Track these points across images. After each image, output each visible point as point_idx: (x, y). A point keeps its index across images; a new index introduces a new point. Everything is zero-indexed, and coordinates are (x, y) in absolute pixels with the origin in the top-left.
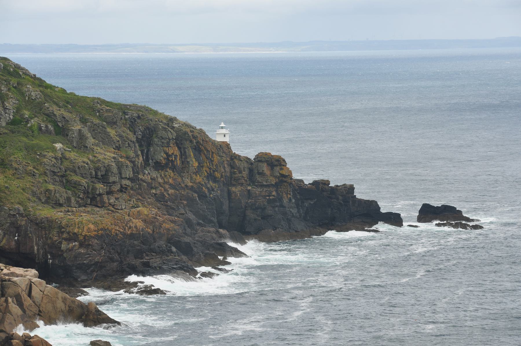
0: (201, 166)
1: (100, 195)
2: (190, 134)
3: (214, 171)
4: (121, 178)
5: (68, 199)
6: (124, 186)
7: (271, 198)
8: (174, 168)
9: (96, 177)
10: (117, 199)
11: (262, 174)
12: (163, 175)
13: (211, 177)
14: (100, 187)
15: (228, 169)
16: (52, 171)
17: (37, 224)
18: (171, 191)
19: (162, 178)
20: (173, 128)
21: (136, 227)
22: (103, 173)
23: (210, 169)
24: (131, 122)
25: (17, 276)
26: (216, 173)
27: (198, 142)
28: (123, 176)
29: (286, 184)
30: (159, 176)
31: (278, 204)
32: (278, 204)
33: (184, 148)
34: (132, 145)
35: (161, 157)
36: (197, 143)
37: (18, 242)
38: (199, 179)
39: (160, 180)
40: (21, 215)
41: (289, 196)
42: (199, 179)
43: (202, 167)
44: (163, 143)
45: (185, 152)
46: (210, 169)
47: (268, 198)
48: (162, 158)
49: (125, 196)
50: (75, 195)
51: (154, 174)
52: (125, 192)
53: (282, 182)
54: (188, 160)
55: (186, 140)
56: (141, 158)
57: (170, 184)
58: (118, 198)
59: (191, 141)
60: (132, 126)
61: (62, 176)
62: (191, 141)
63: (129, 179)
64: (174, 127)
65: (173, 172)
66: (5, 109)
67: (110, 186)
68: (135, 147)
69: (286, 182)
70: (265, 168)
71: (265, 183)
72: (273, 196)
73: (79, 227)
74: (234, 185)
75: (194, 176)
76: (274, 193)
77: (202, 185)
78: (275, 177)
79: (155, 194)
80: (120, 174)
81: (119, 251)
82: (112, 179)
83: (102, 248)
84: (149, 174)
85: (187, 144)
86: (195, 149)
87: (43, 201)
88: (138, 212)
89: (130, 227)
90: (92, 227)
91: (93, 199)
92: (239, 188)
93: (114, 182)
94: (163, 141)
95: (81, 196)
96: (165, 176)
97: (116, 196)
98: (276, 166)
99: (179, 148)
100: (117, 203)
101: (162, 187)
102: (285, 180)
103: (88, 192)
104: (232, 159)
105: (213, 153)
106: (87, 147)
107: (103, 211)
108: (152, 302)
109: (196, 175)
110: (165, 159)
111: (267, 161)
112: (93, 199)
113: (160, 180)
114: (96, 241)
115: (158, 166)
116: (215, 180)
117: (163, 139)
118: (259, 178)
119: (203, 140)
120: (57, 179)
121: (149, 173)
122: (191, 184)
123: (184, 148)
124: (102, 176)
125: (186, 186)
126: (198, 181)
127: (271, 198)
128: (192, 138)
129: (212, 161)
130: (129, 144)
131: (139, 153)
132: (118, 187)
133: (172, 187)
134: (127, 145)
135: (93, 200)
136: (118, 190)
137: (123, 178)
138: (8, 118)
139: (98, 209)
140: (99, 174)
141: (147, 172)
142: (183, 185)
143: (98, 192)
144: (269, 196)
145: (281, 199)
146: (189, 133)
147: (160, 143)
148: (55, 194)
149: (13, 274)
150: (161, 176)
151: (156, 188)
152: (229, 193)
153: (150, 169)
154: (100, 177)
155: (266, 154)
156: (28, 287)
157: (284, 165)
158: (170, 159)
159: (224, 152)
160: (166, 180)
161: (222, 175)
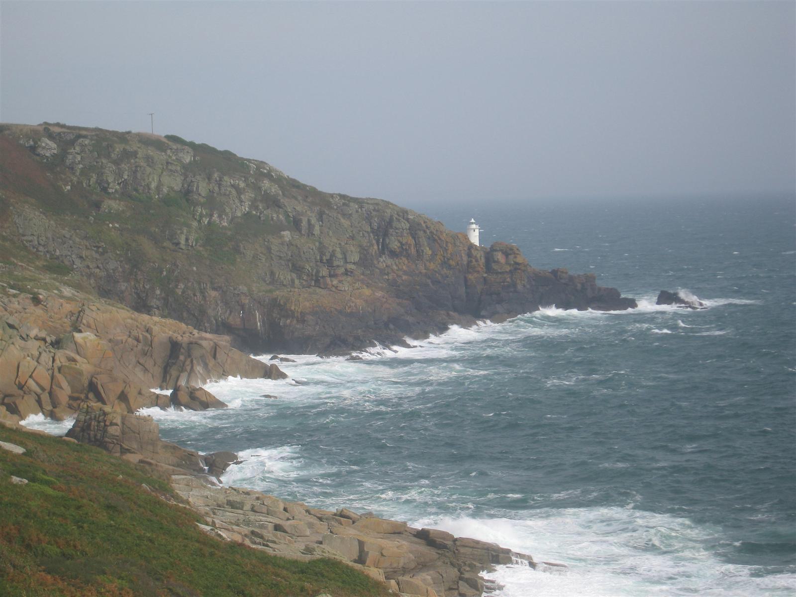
0: (434, 254)
1: (323, 277)
2: (424, 225)
3: (448, 259)
4: (346, 262)
5: (293, 281)
6: (349, 270)
7: (505, 284)
8: (408, 256)
9: (321, 261)
10: (340, 282)
11: (497, 262)
12: (397, 263)
13: (445, 263)
14: (324, 271)
15: (465, 258)
16: (278, 256)
17: (259, 302)
18: (404, 277)
19: (397, 265)
20: (408, 220)
21: (356, 306)
22: (328, 257)
23: (444, 257)
24: (368, 214)
25: (206, 339)
26: (451, 261)
27: (431, 232)
28: (348, 261)
29: (519, 271)
30: (393, 263)
31: (512, 290)
32: (512, 290)
33: (419, 238)
34: (366, 234)
35: (395, 245)
36: (431, 232)
37: (243, 319)
38: (432, 266)
39: (395, 267)
40: (245, 294)
41: (523, 282)
42: (432, 266)
43: (436, 255)
44: (397, 233)
45: (419, 242)
46: (444, 257)
47: (502, 284)
48: (396, 247)
49: (349, 279)
50: (300, 278)
51: (389, 261)
52: (350, 276)
53: (516, 269)
54: (422, 248)
55: (420, 230)
56: (376, 247)
57: (404, 271)
58: (342, 281)
59: (425, 232)
60: (368, 218)
61: (289, 260)
62: (425, 232)
63: (354, 263)
64: (409, 219)
65: (408, 259)
66: (241, 201)
67: (334, 270)
68: (369, 236)
69: (520, 269)
70: (500, 256)
71: (499, 271)
72: (508, 282)
73: (295, 305)
74: (470, 273)
75: (428, 264)
76: (508, 280)
77: (435, 271)
78: (510, 265)
79: (388, 280)
80: (346, 259)
81: (333, 327)
82: (336, 263)
83: (317, 324)
84: (385, 261)
85: (421, 233)
86: (429, 238)
87: (268, 282)
88: (360, 293)
89: (350, 307)
90: (307, 304)
91: (317, 281)
92: (476, 275)
93: (338, 266)
94: (397, 231)
95: (305, 278)
96: (400, 263)
97: (340, 278)
98: (510, 254)
99: (414, 238)
100: (340, 285)
101: (395, 273)
102: (520, 267)
103: (312, 275)
104: (469, 249)
105: (447, 242)
106: (314, 235)
107: (324, 292)
108: (663, 468)
109: (430, 262)
110: (399, 247)
111: (502, 251)
112: (317, 281)
113: (395, 267)
114: (311, 317)
115: (393, 254)
116: (450, 267)
117: (397, 229)
118: (495, 266)
119: (437, 230)
120: (283, 263)
121: (384, 261)
122: (424, 271)
123: (419, 238)
124: (326, 260)
125: (420, 273)
126: (431, 268)
127: (505, 284)
128: (425, 227)
129: (446, 250)
130: (363, 234)
131: (374, 242)
132: (342, 270)
133: (405, 273)
134: (361, 235)
135: (318, 281)
136: (342, 274)
137: (348, 263)
138: (244, 210)
139: (320, 290)
140: (324, 258)
141: (382, 260)
142: (417, 272)
143: (321, 275)
144: (504, 282)
145: (514, 285)
146: (422, 223)
147: (394, 233)
148: (279, 275)
149: (202, 338)
150: (395, 263)
151: (388, 274)
152: (466, 280)
153: (385, 257)
154: (325, 261)
155: (205, 144)
156: (213, 350)
157: (518, 254)
158: (404, 247)
159: (461, 242)
160: (400, 267)
161: (458, 263)
